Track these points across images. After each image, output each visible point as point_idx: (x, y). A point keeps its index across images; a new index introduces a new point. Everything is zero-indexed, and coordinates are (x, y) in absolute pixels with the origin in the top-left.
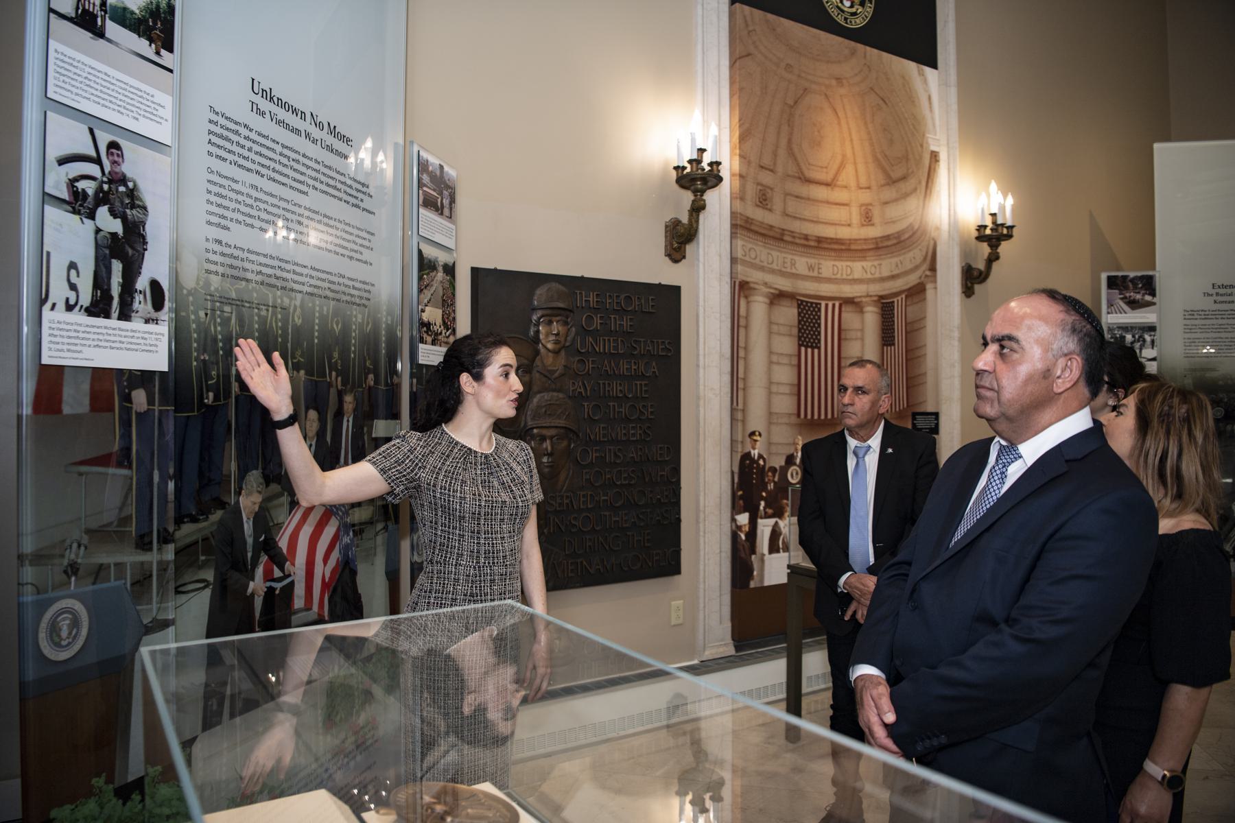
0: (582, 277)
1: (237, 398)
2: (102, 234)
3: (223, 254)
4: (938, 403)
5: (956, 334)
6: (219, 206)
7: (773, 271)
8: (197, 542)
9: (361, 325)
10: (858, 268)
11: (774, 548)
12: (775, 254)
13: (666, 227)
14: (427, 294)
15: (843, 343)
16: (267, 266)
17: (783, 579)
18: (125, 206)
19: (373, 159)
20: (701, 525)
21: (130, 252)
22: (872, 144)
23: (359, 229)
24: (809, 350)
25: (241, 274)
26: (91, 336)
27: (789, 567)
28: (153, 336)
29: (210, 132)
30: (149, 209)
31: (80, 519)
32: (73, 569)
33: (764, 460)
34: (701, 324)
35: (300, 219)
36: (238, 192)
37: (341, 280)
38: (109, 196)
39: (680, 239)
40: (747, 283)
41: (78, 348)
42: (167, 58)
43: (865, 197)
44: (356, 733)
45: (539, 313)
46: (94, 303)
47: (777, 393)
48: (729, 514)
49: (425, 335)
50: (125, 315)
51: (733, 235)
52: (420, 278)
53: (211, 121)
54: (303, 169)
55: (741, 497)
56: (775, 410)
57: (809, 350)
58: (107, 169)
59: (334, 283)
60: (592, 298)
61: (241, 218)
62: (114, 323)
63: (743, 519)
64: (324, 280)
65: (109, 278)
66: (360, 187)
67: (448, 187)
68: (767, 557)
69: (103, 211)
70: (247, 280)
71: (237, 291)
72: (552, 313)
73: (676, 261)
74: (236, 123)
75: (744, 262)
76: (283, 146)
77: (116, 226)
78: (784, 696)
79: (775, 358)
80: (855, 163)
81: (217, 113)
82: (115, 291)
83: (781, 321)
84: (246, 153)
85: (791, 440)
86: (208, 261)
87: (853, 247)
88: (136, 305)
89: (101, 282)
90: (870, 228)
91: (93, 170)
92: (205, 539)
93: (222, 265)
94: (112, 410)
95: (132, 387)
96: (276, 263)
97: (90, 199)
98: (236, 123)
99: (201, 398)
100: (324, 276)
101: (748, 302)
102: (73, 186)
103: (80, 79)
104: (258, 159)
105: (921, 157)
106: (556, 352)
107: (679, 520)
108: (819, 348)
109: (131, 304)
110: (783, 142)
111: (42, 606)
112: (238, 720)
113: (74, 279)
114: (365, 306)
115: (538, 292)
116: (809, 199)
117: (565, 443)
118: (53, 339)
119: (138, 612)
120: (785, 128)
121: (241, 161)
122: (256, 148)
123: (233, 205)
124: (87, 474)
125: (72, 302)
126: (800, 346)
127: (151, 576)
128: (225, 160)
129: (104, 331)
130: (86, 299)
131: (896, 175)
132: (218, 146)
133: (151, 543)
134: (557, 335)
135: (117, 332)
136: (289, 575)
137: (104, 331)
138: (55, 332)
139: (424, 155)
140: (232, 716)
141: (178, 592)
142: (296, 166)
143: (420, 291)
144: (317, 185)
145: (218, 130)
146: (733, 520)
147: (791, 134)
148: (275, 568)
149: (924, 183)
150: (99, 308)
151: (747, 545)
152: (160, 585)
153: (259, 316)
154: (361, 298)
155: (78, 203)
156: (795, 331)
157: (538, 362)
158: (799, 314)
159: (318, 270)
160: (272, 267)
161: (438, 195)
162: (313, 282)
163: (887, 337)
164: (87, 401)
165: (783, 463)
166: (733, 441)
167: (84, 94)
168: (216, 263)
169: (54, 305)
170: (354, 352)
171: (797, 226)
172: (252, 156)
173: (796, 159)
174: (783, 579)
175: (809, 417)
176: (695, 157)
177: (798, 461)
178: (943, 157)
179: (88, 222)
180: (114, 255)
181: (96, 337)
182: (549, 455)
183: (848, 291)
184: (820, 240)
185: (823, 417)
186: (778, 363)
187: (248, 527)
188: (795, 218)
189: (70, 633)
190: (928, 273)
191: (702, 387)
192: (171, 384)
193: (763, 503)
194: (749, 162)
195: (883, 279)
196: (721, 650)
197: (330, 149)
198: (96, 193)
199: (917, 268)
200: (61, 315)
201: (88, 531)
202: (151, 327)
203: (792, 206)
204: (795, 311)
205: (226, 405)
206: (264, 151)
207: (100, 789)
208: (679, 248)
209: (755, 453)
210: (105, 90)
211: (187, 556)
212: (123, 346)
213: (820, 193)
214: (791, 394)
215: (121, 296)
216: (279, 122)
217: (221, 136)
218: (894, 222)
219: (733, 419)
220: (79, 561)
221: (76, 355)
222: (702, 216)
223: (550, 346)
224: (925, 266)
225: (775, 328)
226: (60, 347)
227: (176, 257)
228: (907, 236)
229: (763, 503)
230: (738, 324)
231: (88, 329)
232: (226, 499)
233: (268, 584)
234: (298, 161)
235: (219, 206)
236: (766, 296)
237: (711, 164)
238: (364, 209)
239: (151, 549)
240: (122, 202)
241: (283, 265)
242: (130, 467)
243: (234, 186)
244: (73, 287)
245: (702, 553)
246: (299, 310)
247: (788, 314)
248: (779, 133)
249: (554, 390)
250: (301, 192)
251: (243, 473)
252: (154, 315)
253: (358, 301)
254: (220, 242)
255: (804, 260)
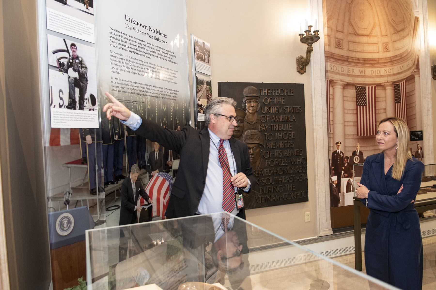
0: (263, 83)
1: (127, 137)
2: (71, 78)
3: (118, 83)
4: (422, 127)
5: (430, 96)
6: (115, 65)
7: (344, 75)
8: (114, 191)
9: (174, 107)
10: (383, 71)
11: (348, 190)
12: (345, 67)
13: (297, 59)
14: (200, 94)
15: (377, 103)
16: (136, 87)
17: (352, 203)
18: (79, 67)
19: (176, 43)
20: (317, 181)
21: (82, 84)
22: (387, 17)
23: (171, 70)
24: (362, 107)
25: (126, 90)
26: (69, 117)
27: (354, 198)
28: (93, 115)
29: (110, 37)
30: (88, 68)
31: (69, 184)
32: (67, 202)
33: (343, 154)
34: (313, 99)
35: (148, 68)
36: (122, 59)
37: (165, 90)
38: (72, 63)
39: (303, 64)
40: (333, 80)
41: (65, 121)
42: (91, 10)
43: (385, 39)
44: (179, 263)
45: (246, 98)
46: (70, 104)
47: (348, 126)
48: (329, 177)
49: (200, 110)
50: (81, 108)
51: (326, 61)
52: (197, 88)
53: (110, 33)
54: (148, 48)
55: (333, 169)
56: (346, 133)
57: (362, 107)
58: (71, 54)
59: (162, 91)
60: (267, 91)
61: (124, 69)
62: (77, 111)
63: (335, 178)
64: (158, 91)
65: (75, 95)
66: (171, 54)
67: (207, 51)
68: (346, 194)
69: (71, 70)
70: (128, 92)
71: (124, 96)
72: (251, 98)
73: (302, 74)
74: (120, 33)
75: (331, 72)
76: (139, 40)
77: (76, 75)
78: (354, 252)
79: (346, 111)
80: (380, 25)
81: (113, 29)
82: (77, 99)
83: (349, 96)
84: (125, 44)
85: (354, 145)
86: (113, 86)
87: (380, 62)
88: (85, 104)
89: (71, 96)
90: (388, 53)
91: (66, 54)
92: (117, 190)
93: (118, 87)
94: (79, 144)
95: (86, 135)
96: (139, 85)
97: (66, 66)
98: (120, 33)
99: (113, 137)
100: (158, 89)
101: (333, 89)
102: (59, 61)
103: (59, 21)
104: (129, 46)
105: (410, 20)
106: (253, 114)
107: (307, 179)
108: (366, 106)
109: (84, 104)
110: (347, 19)
111: (56, 216)
112: (132, 258)
113: (61, 96)
114: (176, 100)
115: (245, 90)
116: (359, 43)
117: (258, 150)
118: (55, 118)
119: (92, 218)
120: (347, 13)
121: (123, 47)
122: (129, 41)
123: (121, 64)
124: (71, 167)
125: (61, 104)
126: (357, 105)
127: (97, 204)
128: (117, 47)
129: (74, 114)
130: (66, 103)
131: (399, 29)
132: (114, 42)
133: (96, 192)
134: (253, 107)
135: (79, 114)
136: (150, 203)
137: (74, 114)
138: (56, 116)
139: (196, 39)
140: (130, 257)
141: (107, 210)
142: (145, 47)
143: (197, 92)
144: (154, 54)
145: (113, 36)
146: (330, 179)
147: (350, 15)
148: (145, 201)
149: (412, 31)
150: (71, 106)
151: (337, 189)
152: (100, 208)
153: (133, 105)
154: (174, 97)
155: (61, 68)
156: (355, 99)
157: (246, 118)
158: (356, 92)
159: (156, 87)
160: (138, 87)
161: (203, 56)
162: (154, 92)
163: (397, 99)
164: (69, 141)
165: (351, 155)
166: (329, 147)
167: (61, 27)
168: (116, 87)
169: (55, 106)
170: (172, 118)
171: (354, 55)
172: (127, 45)
173: (353, 26)
174: (352, 203)
175: (362, 135)
176: (308, 29)
177: (358, 154)
178: (421, 19)
179: (65, 74)
180: (76, 86)
181: (71, 117)
182: (252, 155)
183: (378, 81)
184: (364, 60)
185: (369, 135)
186: (348, 113)
187: (134, 186)
188: (353, 51)
189: (67, 226)
190: (415, 70)
191: (314, 125)
192: (101, 133)
193: (343, 172)
194: (332, 30)
195: (394, 75)
196: (327, 232)
197: (158, 39)
198: (68, 63)
199: (410, 69)
200: (57, 108)
201: (73, 188)
202: (92, 112)
203: (352, 46)
204: (355, 91)
205: (123, 140)
206: (132, 43)
207: (81, 282)
208: (303, 68)
209: (339, 151)
210: (68, 24)
211: (110, 197)
212: (81, 120)
213: (364, 39)
214: (354, 126)
215: (79, 101)
216: (137, 31)
217: (115, 38)
218: (399, 49)
219: (329, 137)
220: (70, 199)
221: (64, 124)
222: (312, 54)
223: (250, 111)
224: (414, 67)
225: (346, 99)
226: (58, 121)
227: (99, 86)
228: (405, 55)
229: (343, 172)
230: (329, 98)
231: (68, 114)
232: (124, 175)
233: (142, 207)
234: (145, 45)
235: (115, 65)
236: (341, 85)
237: (314, 32)
238: (173, 62)
239: (96, 194)
240: (78, 66)
241: (142, 86)
242: (86, 164)
243: (121, 57)
244: (61, 99)
245: (317, 193)
246: (149, 103)
247: (352, 92)
248: (345, 15)
249: (253, 129)
250: (147, 57)
251: (130, 166)
252: (92, 107)
253: (172, 98)
254: (117, 79)
255: (358, 69)
